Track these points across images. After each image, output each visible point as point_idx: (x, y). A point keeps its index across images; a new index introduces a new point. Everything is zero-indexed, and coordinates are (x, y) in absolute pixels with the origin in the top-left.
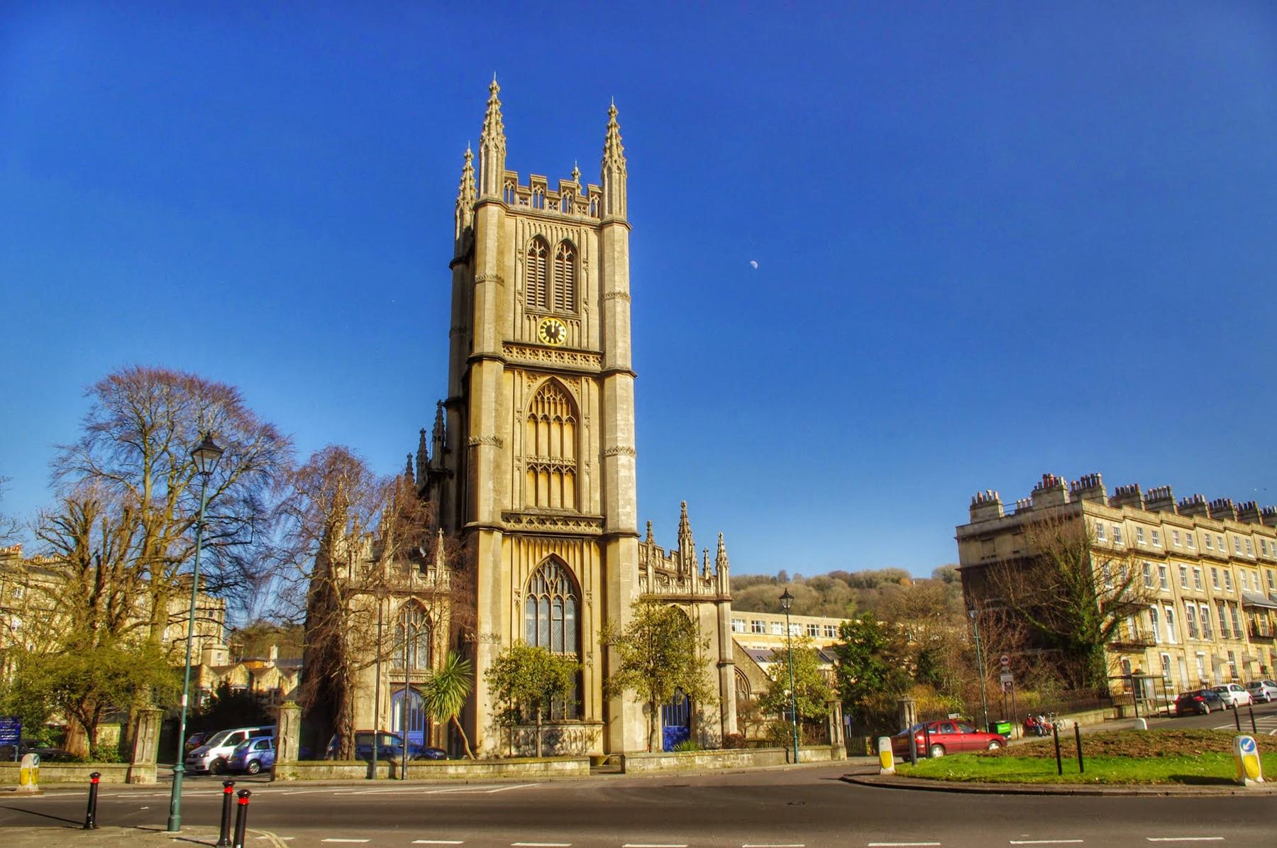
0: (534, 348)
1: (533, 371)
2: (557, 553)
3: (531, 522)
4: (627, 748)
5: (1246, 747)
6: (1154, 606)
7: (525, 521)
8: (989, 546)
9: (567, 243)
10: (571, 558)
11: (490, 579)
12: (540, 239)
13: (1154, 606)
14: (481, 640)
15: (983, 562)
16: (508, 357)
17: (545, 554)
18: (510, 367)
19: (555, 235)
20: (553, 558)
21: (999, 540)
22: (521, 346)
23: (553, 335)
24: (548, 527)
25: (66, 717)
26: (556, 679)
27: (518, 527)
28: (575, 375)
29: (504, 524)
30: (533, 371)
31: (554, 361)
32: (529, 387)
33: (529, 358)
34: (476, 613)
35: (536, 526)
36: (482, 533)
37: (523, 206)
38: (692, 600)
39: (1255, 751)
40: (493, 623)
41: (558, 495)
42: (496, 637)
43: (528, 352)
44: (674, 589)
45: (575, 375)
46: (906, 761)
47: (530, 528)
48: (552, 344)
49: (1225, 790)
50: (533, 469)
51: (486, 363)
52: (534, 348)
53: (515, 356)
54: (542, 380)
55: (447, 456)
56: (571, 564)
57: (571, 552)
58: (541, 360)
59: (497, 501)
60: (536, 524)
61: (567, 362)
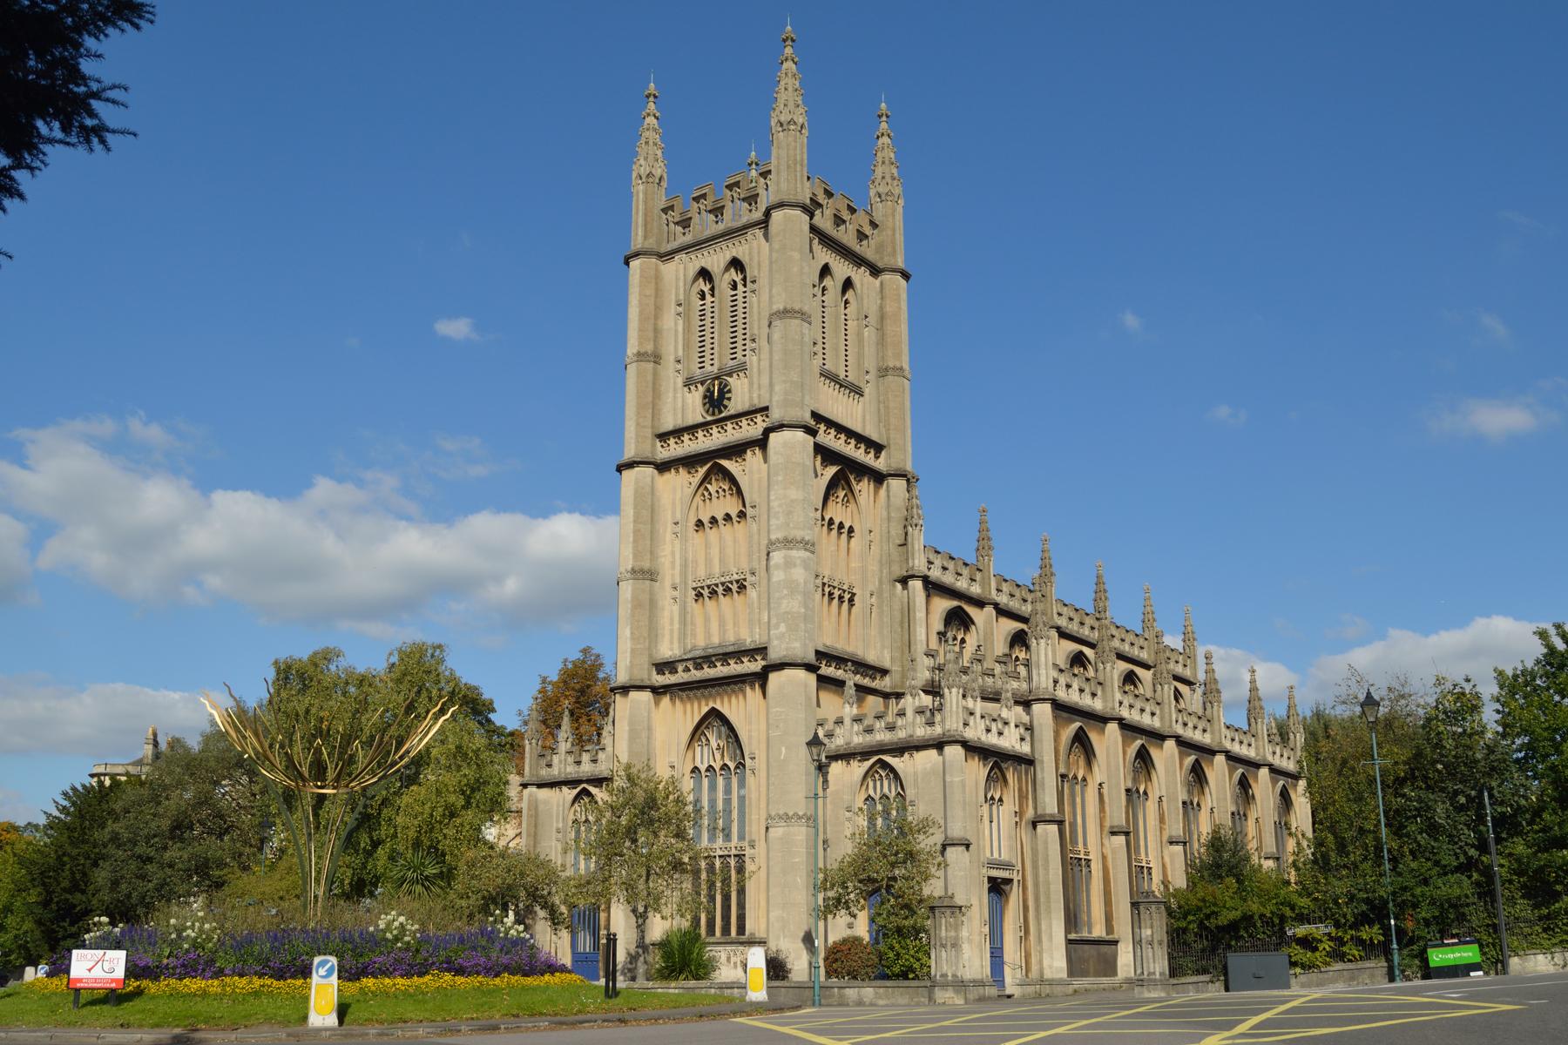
0: (692, 429)
1: (690, 462)
2: (718, 707)
7: (680, 668)
12: (704, 274)
17: (705, 709)
22: (677, 433)
24: (708, 672)
28: (736, 450)
30: (690, 462)
33: (689, 446)
38: (900, 749)
45: (736, 450)
54: (702, 471)
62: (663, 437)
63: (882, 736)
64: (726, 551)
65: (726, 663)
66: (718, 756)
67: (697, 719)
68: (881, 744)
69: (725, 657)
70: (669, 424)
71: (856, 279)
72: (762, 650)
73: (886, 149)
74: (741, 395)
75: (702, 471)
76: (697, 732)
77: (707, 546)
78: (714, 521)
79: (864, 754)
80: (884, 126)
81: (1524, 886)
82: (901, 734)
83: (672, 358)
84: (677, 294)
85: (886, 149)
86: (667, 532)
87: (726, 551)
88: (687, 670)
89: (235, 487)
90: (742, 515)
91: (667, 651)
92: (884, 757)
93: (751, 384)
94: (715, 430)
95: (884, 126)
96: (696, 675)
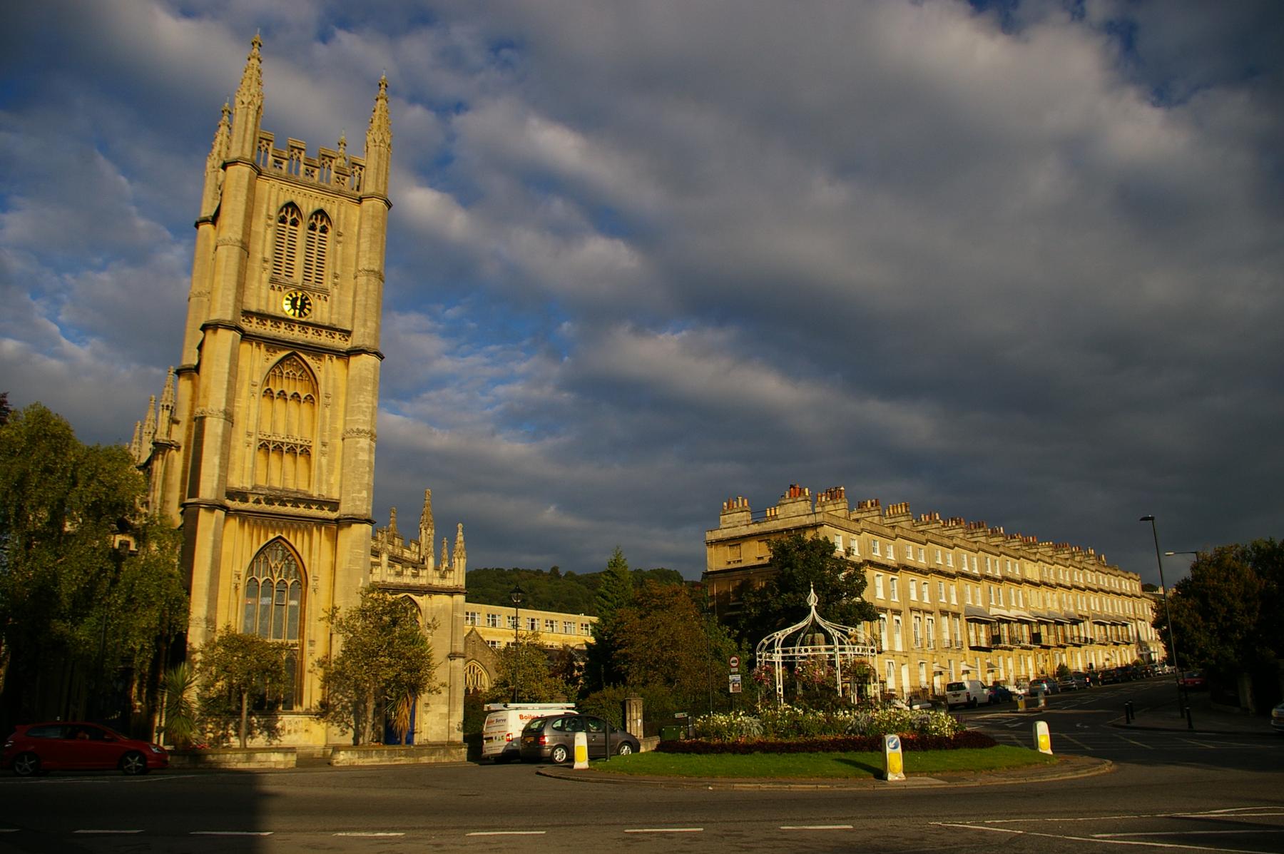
0: (277, 320)
1: (273, 344)
2: (284, 536)
3: (258, 502)
4: (322, 743)
5: (892, 745)
6: (883, 615)
7: (251, 500)
8: (736, 550)
9: (321, 213)
10: (299, 542)
11: (209, 560)
12: (291, 206)
13: (883, 615)
14: (192, 623)
15: (730, 567)
16: (245, 326)
17: (271, 537)
18: (246, 337)
19: (308, 205)
21: (744, 546)
22: (262, 317)
23: (302, 305)
24: (277, 508)
25: (872, 720)
26: (625, 682)
28: (318, 351)
29: (229, 503)
30: (273, 344)
31: (296, 335)
32: (257, 361)
33: (268, 329)
34: (189, 594)
35: (264, 507)
36: (202, 511)
37: (277, 170)
38: (422, 591)
39: (899, 749)
40: (209, 606)
41: (285, 475)
42: (211, 621)
43: (283, 326)
44: (407, 579)
45: (318, 351)
47: (257, 507)
48: (297, 318)
50: (264, 446)
51: (220, 331)
53: (253, 326)
55: (174, 426)
56: (298, 548)
57: (299, 535)
58: (282, 332)
59: (223, 477)
61: (310, 337)
64: (288, 421)
65: (283, 504)
67: (255, 550)
69: (296, 502)
71: (332, 209)
72: (334, 505)
74: (320, 311)
77: (273, 411)
78: (282, 394)
80: (383, 91)
81: (1005, 536)
83: (260, 256)
84: (268, 210)
86: (244, 391)
87: (288, 421)
91: (238, 481)
92: (412, 596)
93: (331, 308)
94: (297, 328)
95: (383, 91)
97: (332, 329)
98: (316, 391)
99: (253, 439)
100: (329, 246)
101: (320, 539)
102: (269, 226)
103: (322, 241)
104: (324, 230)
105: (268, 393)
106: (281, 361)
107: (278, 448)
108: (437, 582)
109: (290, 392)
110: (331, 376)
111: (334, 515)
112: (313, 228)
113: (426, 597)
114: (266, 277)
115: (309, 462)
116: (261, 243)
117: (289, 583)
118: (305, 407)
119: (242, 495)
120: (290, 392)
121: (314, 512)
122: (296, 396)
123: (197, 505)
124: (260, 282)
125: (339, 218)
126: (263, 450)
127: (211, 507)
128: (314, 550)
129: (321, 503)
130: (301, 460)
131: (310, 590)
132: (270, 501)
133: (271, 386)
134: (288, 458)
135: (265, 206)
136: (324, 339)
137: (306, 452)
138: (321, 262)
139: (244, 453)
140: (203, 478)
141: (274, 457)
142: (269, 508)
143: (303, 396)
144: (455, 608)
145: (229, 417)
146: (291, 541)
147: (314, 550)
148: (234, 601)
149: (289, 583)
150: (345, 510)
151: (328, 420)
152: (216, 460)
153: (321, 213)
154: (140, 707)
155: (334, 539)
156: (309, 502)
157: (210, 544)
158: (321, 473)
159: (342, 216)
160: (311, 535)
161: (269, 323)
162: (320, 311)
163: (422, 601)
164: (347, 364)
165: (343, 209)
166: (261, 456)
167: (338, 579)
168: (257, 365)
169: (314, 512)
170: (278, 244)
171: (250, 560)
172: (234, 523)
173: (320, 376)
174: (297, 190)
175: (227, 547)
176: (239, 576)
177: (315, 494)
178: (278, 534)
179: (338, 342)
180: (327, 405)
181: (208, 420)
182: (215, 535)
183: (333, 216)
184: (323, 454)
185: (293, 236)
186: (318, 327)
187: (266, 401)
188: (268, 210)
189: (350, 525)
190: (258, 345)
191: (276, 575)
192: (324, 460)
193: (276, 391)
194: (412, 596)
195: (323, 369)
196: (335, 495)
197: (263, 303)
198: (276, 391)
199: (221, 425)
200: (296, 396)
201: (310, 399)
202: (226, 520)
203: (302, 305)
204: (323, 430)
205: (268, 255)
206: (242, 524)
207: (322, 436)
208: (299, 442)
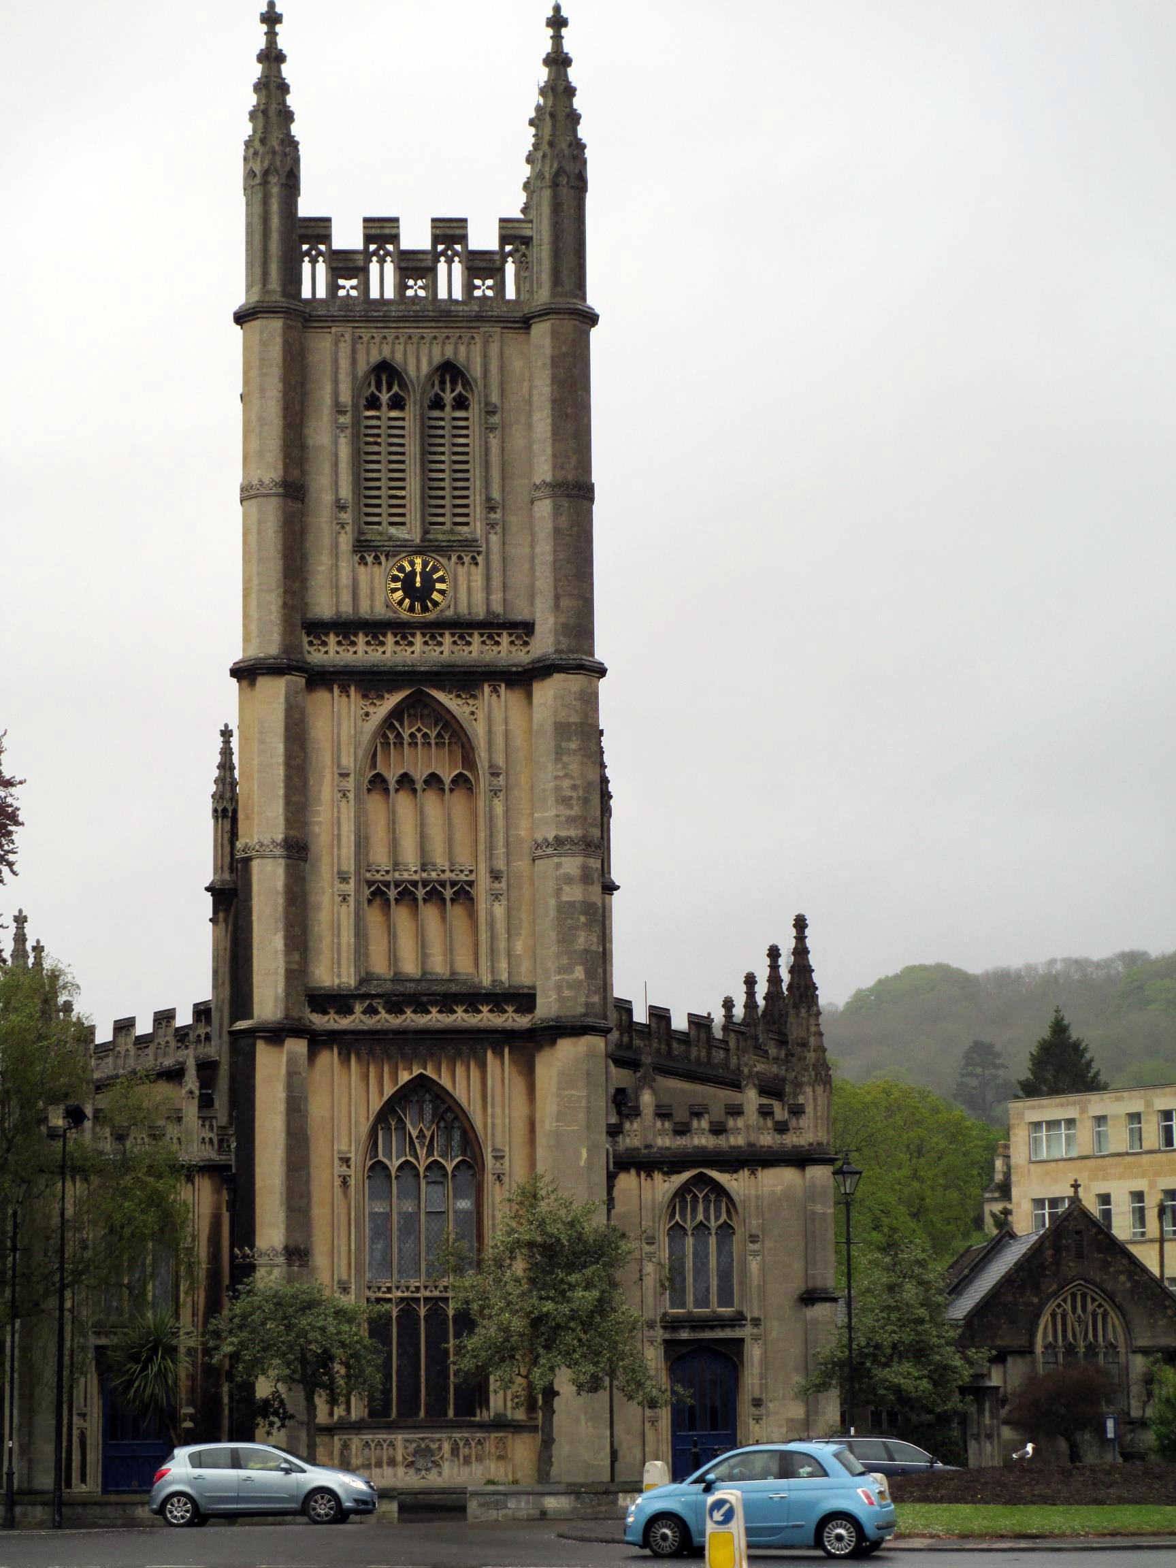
0: (376, 629)
1: (371, 681)
2: (430, 1073)
7: (358, 1008)
9: (449, 371)
10: (459, 1083)
12: (386, 371)
17: (405, 1077)
20: (421, 1082)
22: (346, 628)
23: (418, 592)
24: (411, 1019)
27: (345, 1023)
28: (467, 680)
30: (371, 681)
31: (418, 652)
33: (362, 653)
36: (261, 1047)
41: (422, 947)
45: (467, 680)
46: (331, 1358)
47: (370, 1022)
48: (418, 616)
49: (235, 743)
52: (376, 629)
53: (331, 653)
54: (392, 700)
57: (460, 1070)
58: (388, 653)
59: (297, 974)
60: (383, 1014)
61: (447, 651)
62: (317, 629)
63: (701, 1140)
64: (421, 834)
65: (422, 1009)
66: (422, 1152)
67: (376, 1105)
68: (702, 1149)
69: (447, 1002)
70: (324, 606)
72: (525, 1000)
73: (436, 693)
75: (392, 700)
76: (389, 1115)
78: (405, 781)
79: (671, 1163)
82: (737, 1140)
83: (327, 498)
84: (336, 393)
85: (436, 693)
86: (325, 789)
87: (421, 834)
88: (371, 1011)
89: (263, 72)
90: (461, 782)
91: (333, 970)
92: (714, 1174)
96: (385, 1020)
97: (491, 626)
98: (469, 760)
99: (350, 887)
100: (474, 441)
101: (500, 1070)
102: (342, 428)
103: (460, 429)
104: (461, 403)
105: (378, 783)
106: (396, 714)
107: (407, 894)
108: (767, 1139)
109: (419, 775)
110: (499, 728)
111: (523, 1022)
112: (437, 404)
113: (744, 1174)
114: (346, 541)
115: (472, 915)
116: (327, 468)
117: (449, 1167)
118: (457, 802)
119: (339, 1001)
120: (419, 775)
121: (486, 1018)
122: (433, 780)
123: (251, 1033)
124: (336, 546)
125: (486, 372)
126: (378, 902)
127: (276, 1034)
128: (487, 1092)
129: (499, 999)
130: (457, 913)
131: (489, 1178)
132: (395, 1007)
133: (380, 768)
134: (430, 913)
135: (328, 388)
136: (476, 651)
137: (464, 894)
138: (461, 475)
139: (334, 915)
140: (258, 979)
141: (401, 915)
142: (395, 1021)
143: (447, 777)
144: (811, 1194)
145: (297, 850)
146: (445, 1081)
147: (487, 1092)
148: (343, 1211)
149: (449, 1167)
150: (547, 1007)
151: (500, 823)
152: (278, 941)
153: (449, 371)
154: (192, 1418)
155: (528, 1071)
156: (473, 999)
157: (281, 1107)
158: (493, 937)
159: (494, 367)
160: (483, 1066)
161: (361, 639)
162: (464, 589)
163: (736, 1183)
164: (529, 696)
165: (494, 349)
166: (374, 917)
167: (541, 1152)
168: (347, 730)
169: (486, 1018)
170: (360, 459)
171: (365, 1128)
172: (328, 1059)
173: (478, 732)
174: (390, 335)
175: (318, 1108)
176: (499, 1178)
177: (486, 981)
178: (417, 1071)
179: (506, 652)
180: (495, 793)
181: (255, 864)
182: (289, 1087)
183: (476, 371)
184: (496, 897)
185: (396, 429)
186: (461, 627)
187: (375, 803)
188: (336, 393)
189: (553, 1043)
190: (345, 690)
191: (422, 1152)
192: (499, 910)
193: (392, 779)
194: (714, 1174)
195: (481, 715)
196: (524, 978)
197: (346, 597)
198: (392, 779)
199: (281, 872)
200: (433, 780)
201: (461, 782)
202: (312, 1056)
203: (418, 592)
204: (491, 847)
205: (345, 492)
206: (345, 1060)
207: (491, 857)
208: (447, 875)
